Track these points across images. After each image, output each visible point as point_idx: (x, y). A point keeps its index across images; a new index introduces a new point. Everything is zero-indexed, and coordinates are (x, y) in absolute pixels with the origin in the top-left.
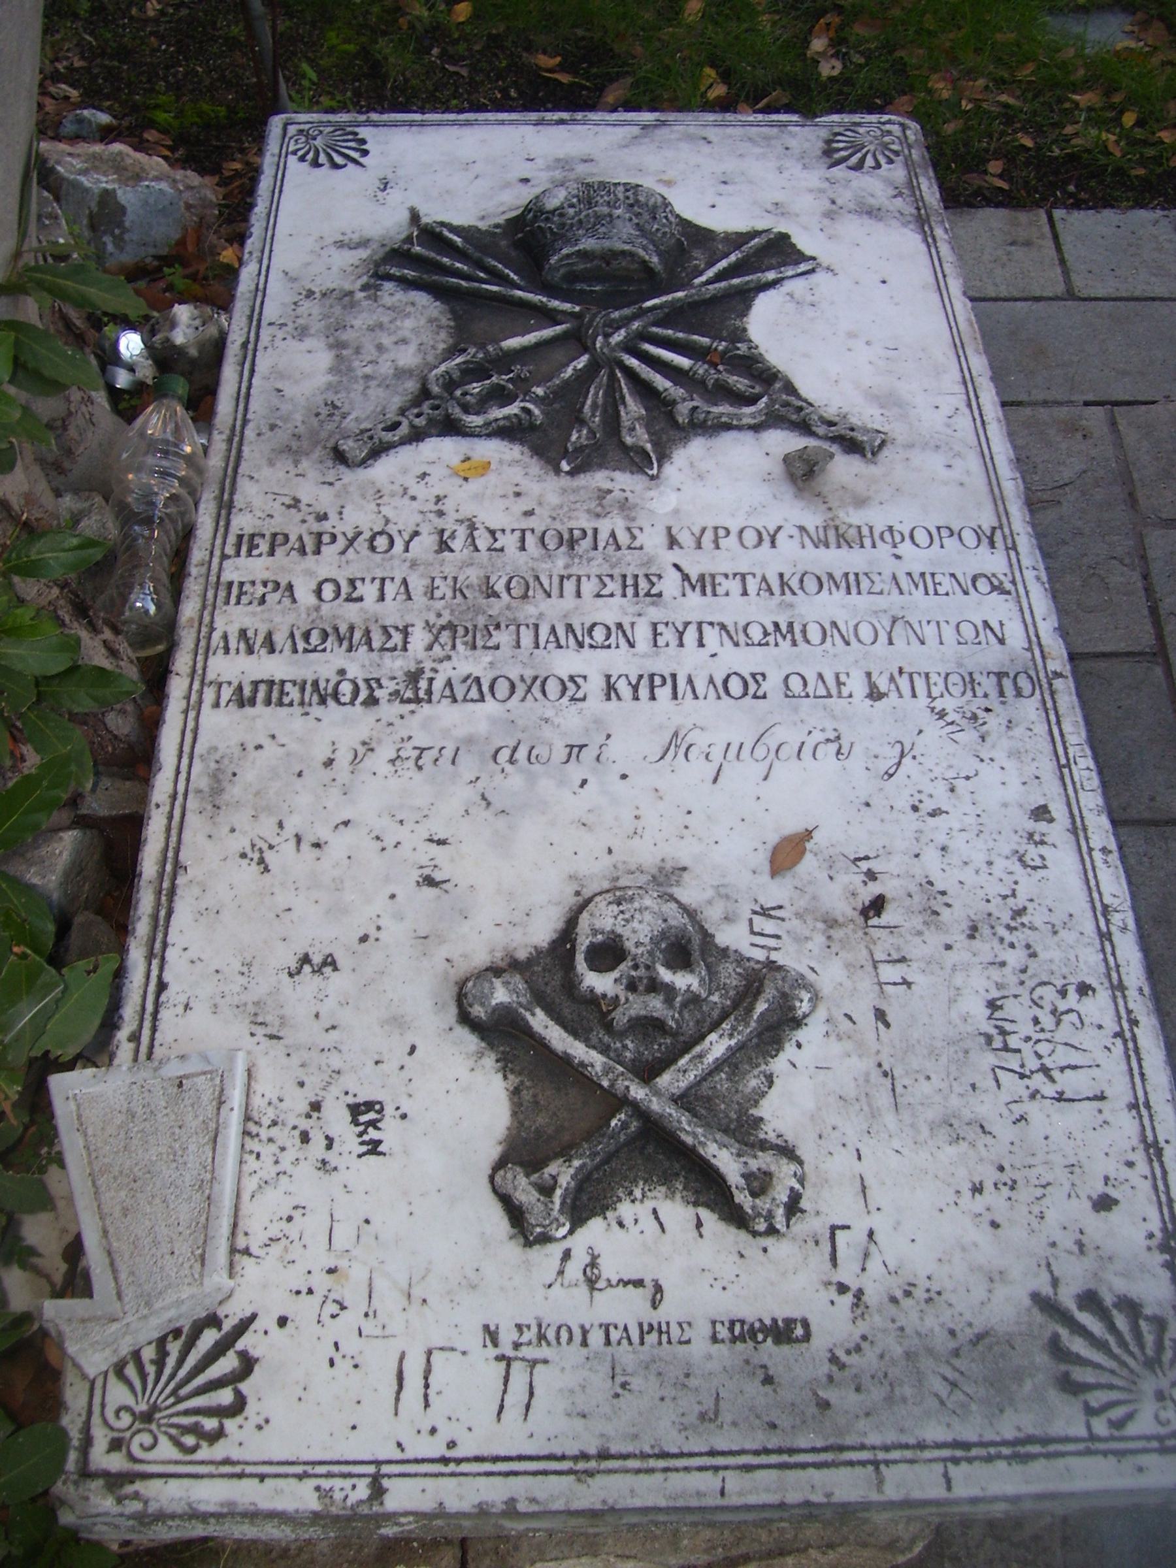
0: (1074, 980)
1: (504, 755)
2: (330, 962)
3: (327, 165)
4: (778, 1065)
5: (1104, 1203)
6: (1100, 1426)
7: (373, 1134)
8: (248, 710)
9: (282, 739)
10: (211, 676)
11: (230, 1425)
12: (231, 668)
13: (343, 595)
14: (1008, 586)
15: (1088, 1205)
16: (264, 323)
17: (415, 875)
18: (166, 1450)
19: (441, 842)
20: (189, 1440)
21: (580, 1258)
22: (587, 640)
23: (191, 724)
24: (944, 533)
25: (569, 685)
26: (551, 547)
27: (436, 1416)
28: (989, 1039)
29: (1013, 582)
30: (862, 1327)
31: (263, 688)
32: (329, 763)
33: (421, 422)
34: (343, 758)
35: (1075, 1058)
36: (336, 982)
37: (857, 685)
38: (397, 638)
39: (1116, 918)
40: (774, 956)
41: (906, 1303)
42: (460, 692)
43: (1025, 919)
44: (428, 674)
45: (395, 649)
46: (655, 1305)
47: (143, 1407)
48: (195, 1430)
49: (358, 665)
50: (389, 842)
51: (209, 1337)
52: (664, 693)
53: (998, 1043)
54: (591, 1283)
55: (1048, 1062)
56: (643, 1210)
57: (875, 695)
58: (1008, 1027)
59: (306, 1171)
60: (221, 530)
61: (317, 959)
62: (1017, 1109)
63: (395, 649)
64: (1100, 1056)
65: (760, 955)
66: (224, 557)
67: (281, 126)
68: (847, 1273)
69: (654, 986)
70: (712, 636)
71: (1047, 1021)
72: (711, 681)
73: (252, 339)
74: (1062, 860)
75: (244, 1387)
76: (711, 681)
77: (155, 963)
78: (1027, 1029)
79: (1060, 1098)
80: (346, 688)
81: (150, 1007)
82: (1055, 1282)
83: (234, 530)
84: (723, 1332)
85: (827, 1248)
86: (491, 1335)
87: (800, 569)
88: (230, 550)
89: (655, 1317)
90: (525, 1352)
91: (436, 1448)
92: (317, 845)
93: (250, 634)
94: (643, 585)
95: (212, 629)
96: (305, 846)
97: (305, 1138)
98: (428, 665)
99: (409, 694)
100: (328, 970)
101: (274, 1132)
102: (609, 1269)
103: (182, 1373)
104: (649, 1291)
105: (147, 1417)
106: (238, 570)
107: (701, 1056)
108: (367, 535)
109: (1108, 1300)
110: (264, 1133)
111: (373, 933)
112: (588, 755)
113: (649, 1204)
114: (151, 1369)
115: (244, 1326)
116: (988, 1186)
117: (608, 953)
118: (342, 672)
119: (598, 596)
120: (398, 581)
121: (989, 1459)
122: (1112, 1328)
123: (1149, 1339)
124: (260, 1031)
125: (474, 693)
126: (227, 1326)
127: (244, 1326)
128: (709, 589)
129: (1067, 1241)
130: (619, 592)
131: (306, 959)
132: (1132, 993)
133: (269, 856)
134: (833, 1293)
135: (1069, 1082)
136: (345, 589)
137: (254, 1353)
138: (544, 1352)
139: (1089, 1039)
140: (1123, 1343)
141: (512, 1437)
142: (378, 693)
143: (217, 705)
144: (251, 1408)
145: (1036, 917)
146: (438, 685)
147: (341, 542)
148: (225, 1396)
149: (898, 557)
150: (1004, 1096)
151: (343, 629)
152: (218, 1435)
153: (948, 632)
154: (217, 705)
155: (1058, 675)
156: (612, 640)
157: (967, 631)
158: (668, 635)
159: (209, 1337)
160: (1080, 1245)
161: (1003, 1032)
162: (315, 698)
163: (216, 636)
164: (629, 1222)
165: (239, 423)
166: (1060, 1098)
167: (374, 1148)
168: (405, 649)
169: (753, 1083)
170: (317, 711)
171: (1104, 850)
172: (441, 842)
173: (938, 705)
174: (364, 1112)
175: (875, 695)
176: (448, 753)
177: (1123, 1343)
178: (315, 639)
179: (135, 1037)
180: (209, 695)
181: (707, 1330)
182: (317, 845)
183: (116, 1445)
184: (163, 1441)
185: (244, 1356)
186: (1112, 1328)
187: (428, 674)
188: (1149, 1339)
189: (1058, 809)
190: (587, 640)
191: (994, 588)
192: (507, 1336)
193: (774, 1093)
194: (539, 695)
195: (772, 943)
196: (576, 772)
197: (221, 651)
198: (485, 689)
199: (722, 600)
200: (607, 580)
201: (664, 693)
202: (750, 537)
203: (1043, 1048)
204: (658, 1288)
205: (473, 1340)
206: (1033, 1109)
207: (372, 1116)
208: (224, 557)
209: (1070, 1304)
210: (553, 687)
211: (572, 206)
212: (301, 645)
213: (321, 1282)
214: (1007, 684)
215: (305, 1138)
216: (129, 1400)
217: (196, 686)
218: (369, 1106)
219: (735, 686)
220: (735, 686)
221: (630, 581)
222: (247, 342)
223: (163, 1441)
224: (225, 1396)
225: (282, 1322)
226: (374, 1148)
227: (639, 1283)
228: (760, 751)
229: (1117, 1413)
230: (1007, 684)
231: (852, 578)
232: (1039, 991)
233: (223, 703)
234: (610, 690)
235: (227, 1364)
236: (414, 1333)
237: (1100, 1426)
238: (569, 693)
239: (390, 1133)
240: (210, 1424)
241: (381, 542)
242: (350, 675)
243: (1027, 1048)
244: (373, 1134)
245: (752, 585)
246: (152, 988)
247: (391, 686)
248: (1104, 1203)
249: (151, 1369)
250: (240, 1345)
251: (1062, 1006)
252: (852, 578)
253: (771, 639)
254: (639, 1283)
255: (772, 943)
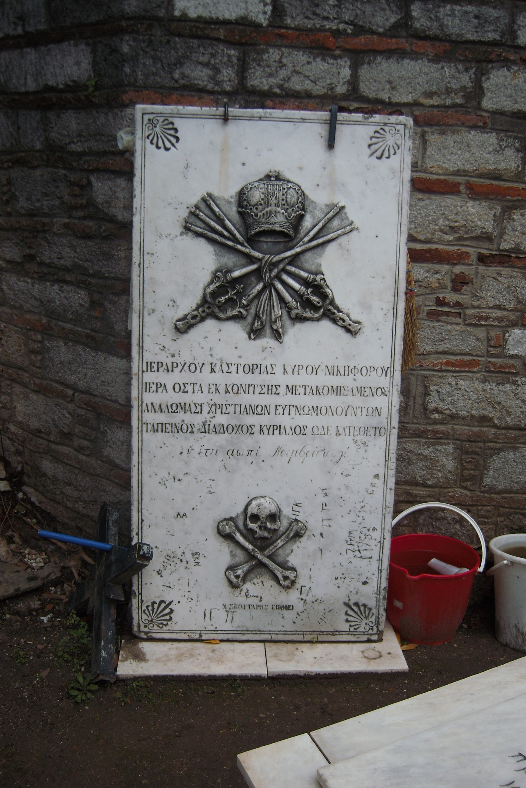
0: (372, 527)
1: (230, 452)
2: (185, 515)
3: (163, 148)
4: (295, 547)
5: (365, 583)
6: (352, 629)
7: (197, 560)
8: (156, 433)
9: (167, 445)
10: (144, 421)
11: (169, 623)
12: (150, 417)
13: (182, 391)
14: (387, 393)
15: (361, 583)
16: (145, 253)
17: (206, 490)
18: (156, 627)
19: (213, 480)
20: (161, 626)
21: (244, 591)
22: (256, 412)
23: (140, 438)
24: (372, 369)
25: (250, 428)
26: (247, 372)
27: (213, 622)
28: (347, 542)
29: (389, 391)
30: (305, 608)
31: (160, 425)
32: (181, 453)
33: (203, 315)
34: (185, 452)
35: (367, 547)
36: (187, 520)
37: (333, 431)
38: (199, 408)
39: (388, 510)
40: (298, 518)
41: (315, 603)
42: (218, 429)
43: (364, 509)
44: (208, 423)
45: (198, 413)
46: (260, 601)
47: (150, 619)
48: (162, 624)
49: (188, 418)
50: (199, 480)
51: (163, 605)
52: (277, 432)
53: (349, 543)
54: (247, 596)
55: (360, 548)
56: (259, 581)
57: (338, 434)
58: (352, 539)
59: (182, 569)
60: (141, 359)
61: (181, 514)
62: (350, 560)
63: (198, 413)
64: (373, 547)
65: (294, 517)
66: (143, 371)
67: (141, 115)
68: (303, 596)
69: (266, 528)
70: (293, 410)
71: (363, 537)
72: (291, 428)
73: (142, 262)
74: (379, 490)
75: (171, 615)
76: (291, 428)
77: (140, 514)
78: (357, 539)
79: (361, 557)
80: (184, 427)
81: (140, 527)
82: (349, 600)
83: (145, 361)
84: (275, 607)
85: (300, 590)
86: (224, 606)
87: (324, 384)
88: (145, 368)
89: (260, 604)
90: (232, 610)
91: (213, 628)
92: (179, 480)
93: (154, 405)
94: (274, 389)
95: (142, 402)
96: (176, 480)
97: (181, 561)
98: (208, 419)
99: (203, 430)
100: (184, 517)
101: (174, 559)
102: (251, 593)
103: (162, 614)
104: (259, 598)
105: (152, 621)
106: (149, 377)
107: (276, 546)
108: (188, 365)
109: (360, 604)
110: (172, 560)
111: (196, 507)
112: (254, 453)
113: (261, 579)
114: (151, 612)
115: (170, 603)
116: (339, 578)
117: (255, 518)
118: (183, 421)
119: (260, 393)
120: (199, 385)
121: (327, 634)
122: (360, 610)
123: (367, 612)
124: (169, 533)
125: (222, 431)
126: (167, 603)
127: (170, 603)
128: (294, 392)
129: (354, 592)
130: (266, 392)
131: (179, 514)
132: (386, 531)
133: (166, 483)
134: (300, 600)
135: (364, 554)
136: (182, 387)
137: (173, 608)
138: (236, 610)
139: (373, 543)
140: (361, 613)
141: (227, 627)
142: (194, 429)
143: (147, 431)
144: (173, 620)
145: (367, 508)
146: (211, 427)
147: (180, 367)
148: (168, 617)
149: (355, 380)
150: (348, 556)
151: (183, 405)
152: (167, 624)
153: (364, 410)
154: (147, 431)
155: (394, 428)
156: (263, 412)
157: (370, 410)
158: (280, 410)
159: (163, 605)
160: (357, 592)
161: (351, 540)
162: (176, 431)
163: (144, 405)
164: (256, 583)
165: (141, 307)
166: (361, 557)
167: (198, 564)
168: (201, 413)
169: (288, 552)
170: (177, 435)
171: (391, 489)
172: (213, 480)
173: (356, 438)
174: (196, 554)
175: (338, 434)
176: (215, 451)
177: (361, 613)
178: (174, 407)
179: (137, 534)
180: (144, 427)
181: (271, 607)
182: (179, 480)
183: (145, 626)
184: (155, 626)
185: (171, 609)
186: (360, 610)
187: (208, 423)
188: (367, 612)
189: (381, 476)
190: (256, 412)
191: (383, 393)
192: (228, 606)
193: (293, 554)
194: (241, 432)
195: (297, 513)
196: (250, 459)
197: (146, 411)
198: (225, 429)
199: (298, 396)
200: (263, 387)
201: (277, 432)
202: (310, 369)
203: (360, 545)
204: (261, 598)
205: (221, 607)
206: (354, 560)
207: (197, 556)
208: (143, 371)
209: (352, 605)
210: (245, 428)
211: (261, 204)
212: (170, 410)
213: (187, 594)
214: (378, 431)
215: (181, 561)
216: (147, 618)
217: (140, 424)
218: (197, 553)
219: (298, 430)
220: (298, 430)
221: (270, 388)
222: (140, 263)
223: (155, 626)
224: (168, 617)
225: (179, 602)
226: (198, 564)
227: (257, 597)
228: (302, 453)
229: (356, 627)
230: (378, 431)
231: (339, 388)
232: (363, 529)
233: (149, 430)
234: (261, 431)
235: (167, 611)
236: (207, 605)
237: (352, 629)
238: (249, 432)
239: (201, 560)
240: (165, 623)
241: (193, 367)
242: (186, 422)
243: (356, 545)
244: (197, 560)
245: (308, 390)
246: (140, 521)
247: (197, 427)
248: (365, 583)
249: (151, 612)
250: (170, 607)
251: (368, 533)
252: (339, 388)
253: (310, 412)
254: (257, 597)
255: (297, 513)
